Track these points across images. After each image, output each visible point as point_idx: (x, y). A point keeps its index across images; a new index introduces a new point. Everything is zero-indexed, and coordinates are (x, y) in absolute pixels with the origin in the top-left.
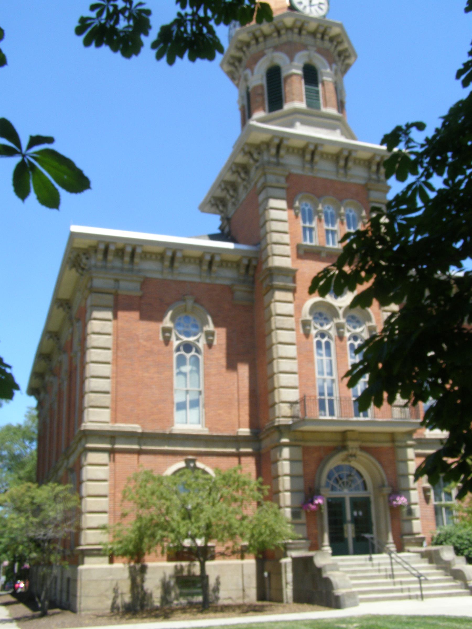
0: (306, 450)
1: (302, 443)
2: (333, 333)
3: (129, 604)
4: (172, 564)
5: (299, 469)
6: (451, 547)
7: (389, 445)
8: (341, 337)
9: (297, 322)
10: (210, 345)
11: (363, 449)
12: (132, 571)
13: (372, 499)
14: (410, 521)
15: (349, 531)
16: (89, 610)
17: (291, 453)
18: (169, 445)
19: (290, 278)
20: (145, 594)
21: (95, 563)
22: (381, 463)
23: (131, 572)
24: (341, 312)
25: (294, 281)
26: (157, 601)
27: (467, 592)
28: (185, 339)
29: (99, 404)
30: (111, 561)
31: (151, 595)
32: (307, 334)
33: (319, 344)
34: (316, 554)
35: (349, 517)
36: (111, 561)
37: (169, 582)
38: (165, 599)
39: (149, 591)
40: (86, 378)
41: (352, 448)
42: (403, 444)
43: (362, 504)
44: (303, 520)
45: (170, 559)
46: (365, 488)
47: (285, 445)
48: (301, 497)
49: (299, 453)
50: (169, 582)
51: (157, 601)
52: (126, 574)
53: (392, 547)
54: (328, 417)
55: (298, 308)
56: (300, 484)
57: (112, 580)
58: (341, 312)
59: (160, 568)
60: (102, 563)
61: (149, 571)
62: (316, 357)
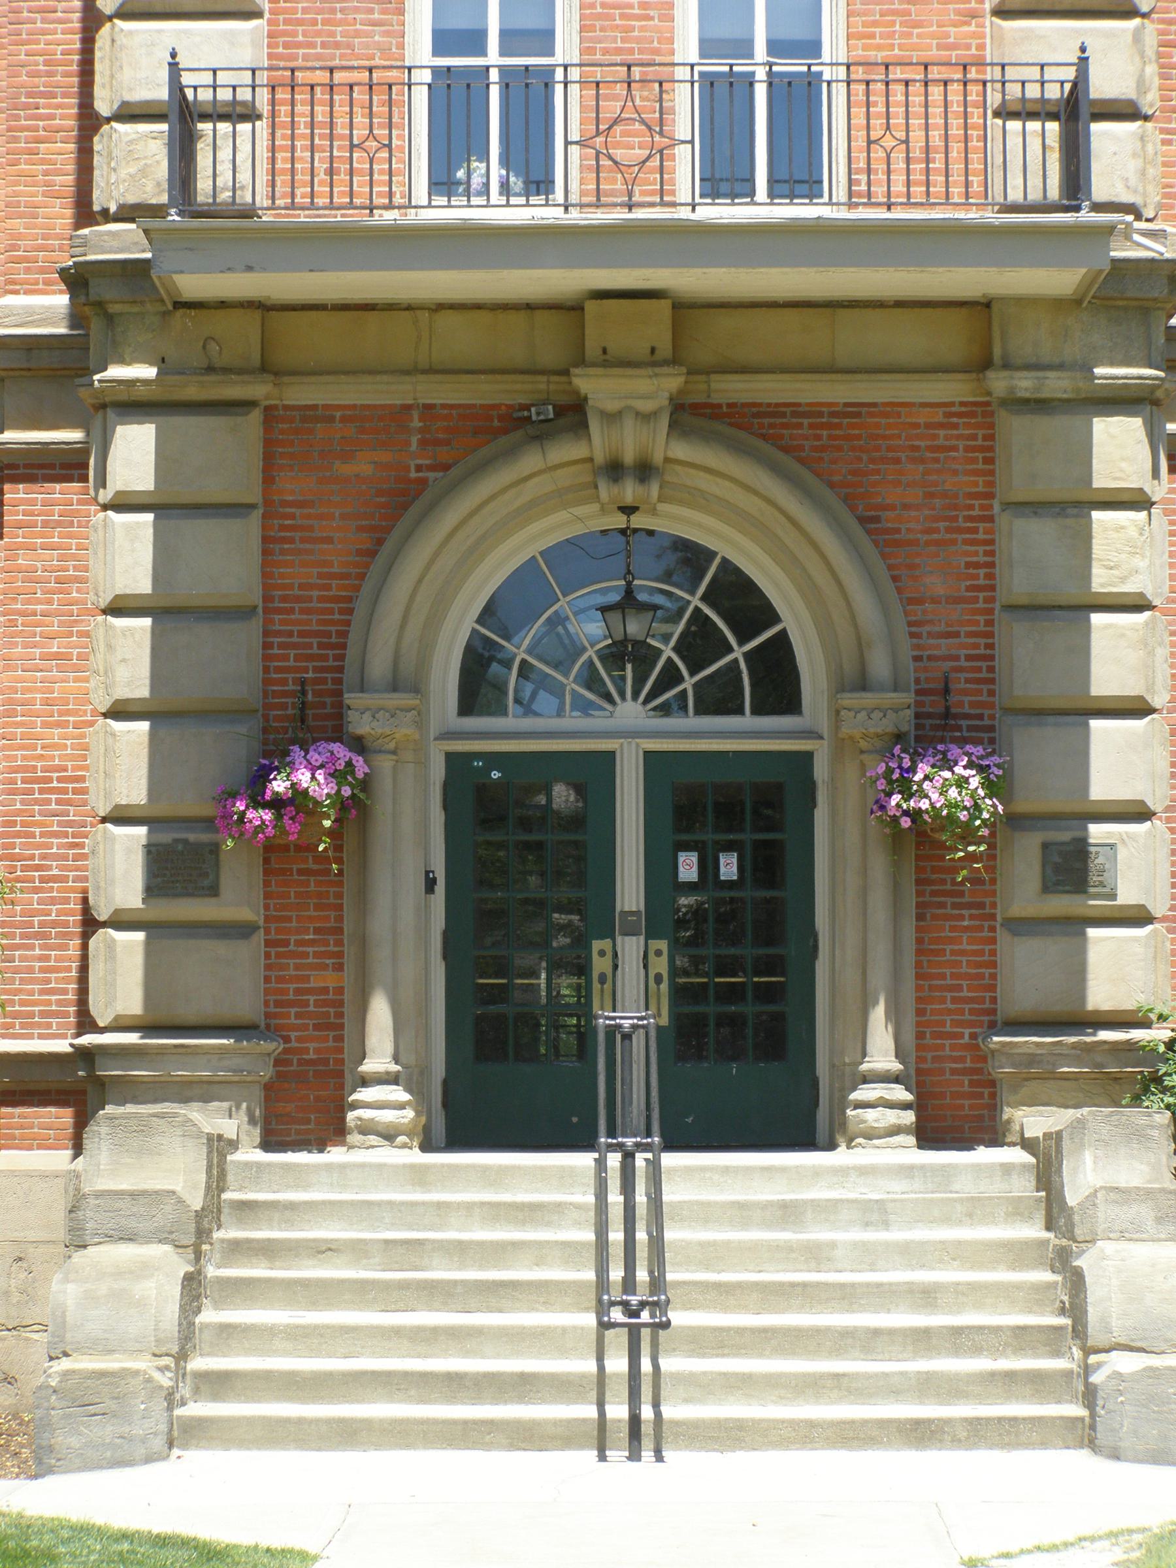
0: (286, 437)
1: (258, 390)
5: (229, 563)
7: (951, 390)
11: (688, 416)
15: (632, 995)
17: (166, 460)
18: (481, 1268)
22: (869, 522)
27: (1024, 1166)
29: (939, 312)
35: (630, 892)
41: (612, 418)
42: (1057, 385)
43: (747, 820)
44: (238, 898)
46: (777, 683)
47: (133, 405)
48: (223, 750)
49: (229, 456)
54: (761, 209)
56: (230, 662)
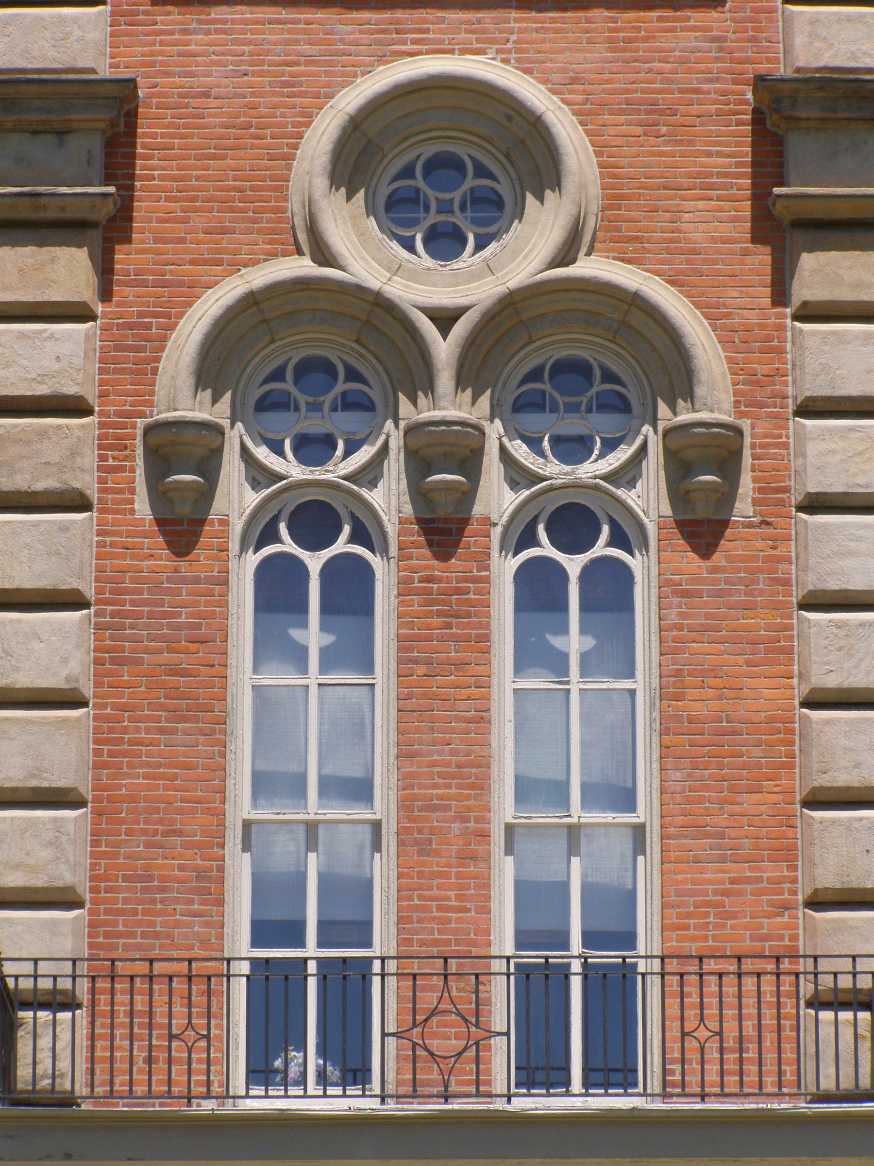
2: (389, 500)
8: (443, 528)
9: (111, 444)
10: (443, 528)
19: (88, 145)
24: (444, 350)
25: (118, 154)
28: (554, 469)
32: (182, 526)
33: (279, 588)
55: (132, 354)
58: (444, 350)
62: (244, 675)
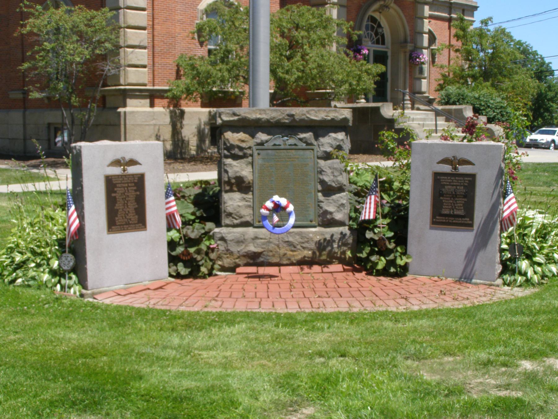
3: (170, 152)
4: (207, 110)
6: (471, 107)
12: (173, 115)
13: (389, 54)
14: (420, 79)
16: (261, 239)
20: (183, 141)
21: (137, 106)
23: (171, 117)
26: (193, 150)
30: (152, 105)
31: (188, 142)
34: (382, 106)
36: (152, 105)
37: (204, 129)
38: (200, 148)
39: (186, 139)
40: (60, 190)
45: (203, 105)
50: (204, 129)
51: (193, 150)
52: (168, 120)
53: (408, 103)
57: (155, 125)
59: (196, 114)
60: (143, 106)
61: (186, 116)
